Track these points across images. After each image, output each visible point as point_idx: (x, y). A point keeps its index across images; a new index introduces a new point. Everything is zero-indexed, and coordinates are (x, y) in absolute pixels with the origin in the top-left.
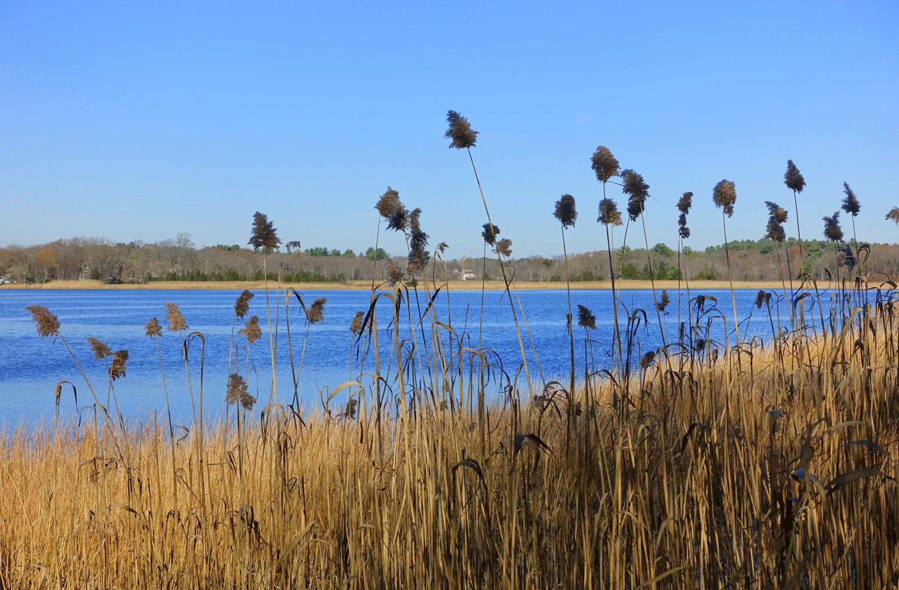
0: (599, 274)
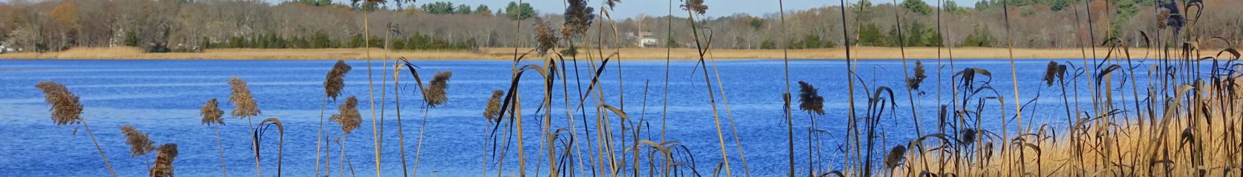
0: (828, 39)
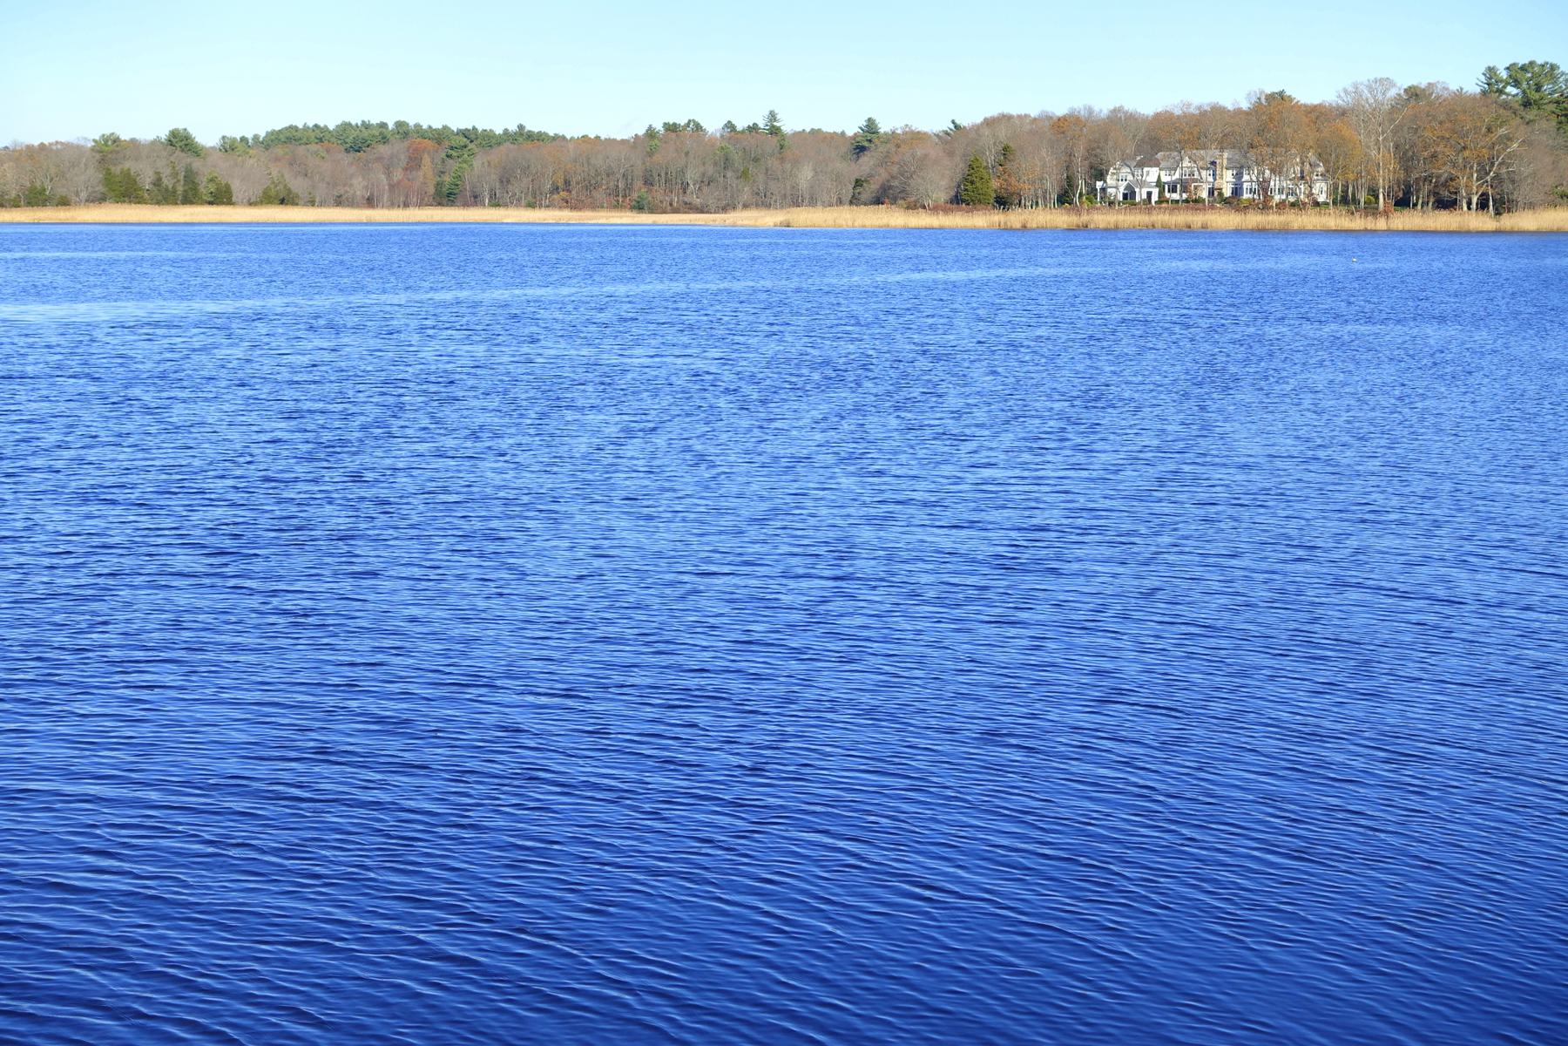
0: (62, 191)
